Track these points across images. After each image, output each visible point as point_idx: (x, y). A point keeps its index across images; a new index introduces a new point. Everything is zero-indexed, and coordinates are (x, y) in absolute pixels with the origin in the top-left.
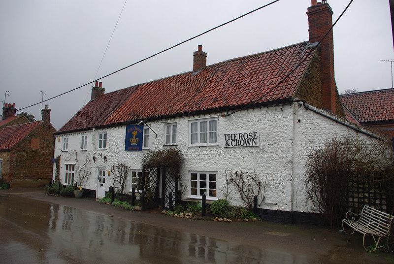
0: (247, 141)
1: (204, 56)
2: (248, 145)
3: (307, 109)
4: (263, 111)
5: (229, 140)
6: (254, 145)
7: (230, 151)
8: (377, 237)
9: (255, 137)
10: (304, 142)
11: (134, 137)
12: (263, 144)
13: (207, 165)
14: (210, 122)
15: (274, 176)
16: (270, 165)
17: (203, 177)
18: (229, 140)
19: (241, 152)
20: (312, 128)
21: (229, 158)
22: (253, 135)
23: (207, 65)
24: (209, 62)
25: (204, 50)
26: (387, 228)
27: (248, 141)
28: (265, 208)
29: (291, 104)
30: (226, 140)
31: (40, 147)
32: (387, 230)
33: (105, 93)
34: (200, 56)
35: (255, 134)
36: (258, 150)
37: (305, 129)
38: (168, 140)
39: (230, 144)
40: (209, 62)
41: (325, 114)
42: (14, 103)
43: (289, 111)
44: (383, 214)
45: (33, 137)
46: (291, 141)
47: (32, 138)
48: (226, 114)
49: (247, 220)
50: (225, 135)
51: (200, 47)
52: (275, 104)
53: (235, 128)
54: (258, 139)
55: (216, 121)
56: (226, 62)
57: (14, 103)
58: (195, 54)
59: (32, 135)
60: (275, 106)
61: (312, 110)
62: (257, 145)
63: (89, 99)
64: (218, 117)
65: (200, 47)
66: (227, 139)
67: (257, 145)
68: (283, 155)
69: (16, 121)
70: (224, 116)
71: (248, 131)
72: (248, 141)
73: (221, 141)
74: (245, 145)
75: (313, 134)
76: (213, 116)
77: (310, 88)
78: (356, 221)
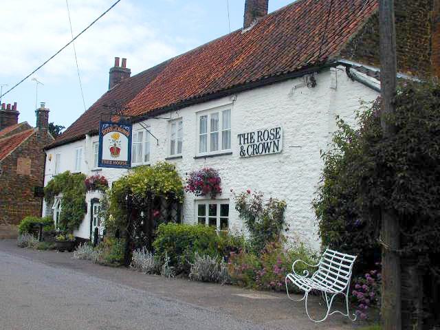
2: (267, 153)
3: (352, 78)
5: (244, 143)
6: (276, 151)
7: (246, 162)
8: (330, 295)
9: (278, 137)
14: (224, 112)
19: (259, 162)
21: (245, 175)
23: (269, 12)
26: (345, 278)
30: (240, 144)
31: (32, 172)
32: (345, 281)
33: (131, 75)
35: (278, 130)
36: (282, 159)
38: (172, 152)
42: (15, 104)
44: (336, 255)
45: (20, 155)
47: (18, 157)
57: (15, 104)
59: (18, 153)
66: (242, 142)
67: (280, 148)
74: (264, 153)
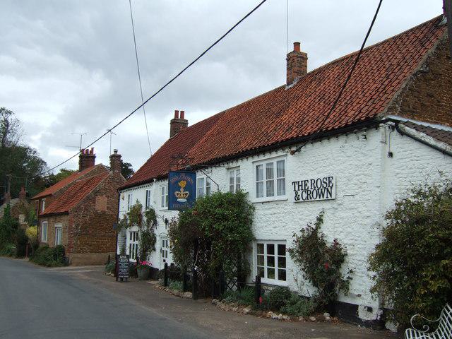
0: (320, 191)
1: (304, 58)
4: (342, 139)
6: (330, 198)
7: (301, 207)
9: (331, 185)
10: (397, 191)
11: (182, 190)
12: (341, 195)
13: (274, 230)
14: (278, 162)
15: (356, 247)
16: (350, 230)
17: (271, 248)
18: (299, 190)
20: (409, 166)
21: (300, 219)
22: (327, 182)
24: (312, 66)
25: (303, 49)
27: (321, 190)
28: (346, 302)
29: (377, 127)
33: (189, 125)
34: (296, 60)
36: (335, 206)
37: (398, 168)
39: (300, 196)
40: (312, 66)
41: (427, 140)
43: (376, 137)
45: (98, 194)
46: (378, 190)
48: (294, 149)
49: (313, 318)
50: (294, 183)
51: (297, 45)
52: (356, 128)
53: (307, 172)
54: (334, 188)
55: (284, 161)
56: (347, 58)
58: (290, 58)
60: (355, 133)
61: (409, 136)
62: (333, 197)
63: (167, 137)
64: (286, 155)
65: (297, 45)
67: (333, 197)
68: (368, 214)
69: (93, 172)
70: (293, 153)
71: (322, 176)
72: (322, 192)
73: (290, 193)
74: (318, 199)
75: (410, 175)
76: (280, 153)
77: (430, 96)
78: (430, 332)
